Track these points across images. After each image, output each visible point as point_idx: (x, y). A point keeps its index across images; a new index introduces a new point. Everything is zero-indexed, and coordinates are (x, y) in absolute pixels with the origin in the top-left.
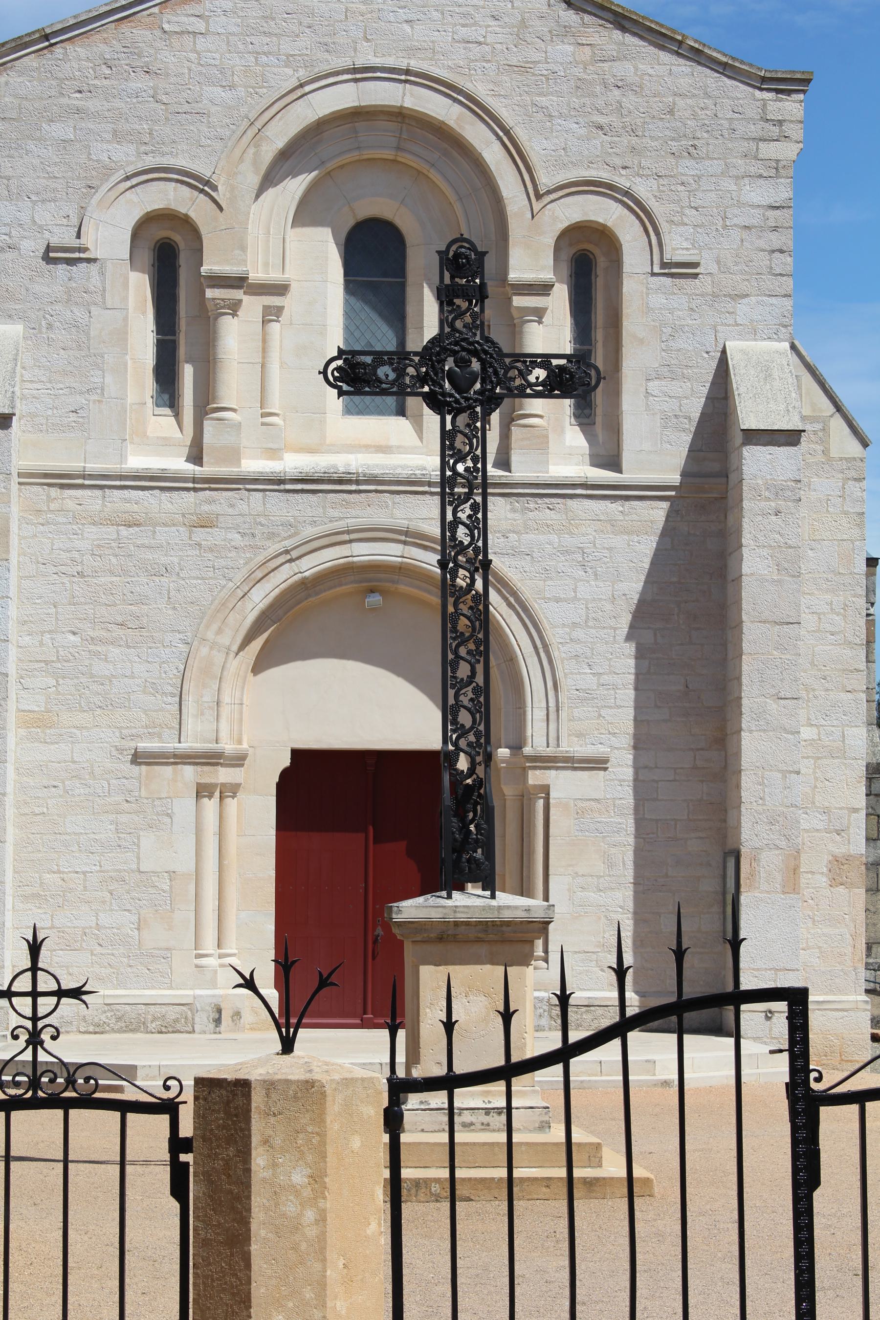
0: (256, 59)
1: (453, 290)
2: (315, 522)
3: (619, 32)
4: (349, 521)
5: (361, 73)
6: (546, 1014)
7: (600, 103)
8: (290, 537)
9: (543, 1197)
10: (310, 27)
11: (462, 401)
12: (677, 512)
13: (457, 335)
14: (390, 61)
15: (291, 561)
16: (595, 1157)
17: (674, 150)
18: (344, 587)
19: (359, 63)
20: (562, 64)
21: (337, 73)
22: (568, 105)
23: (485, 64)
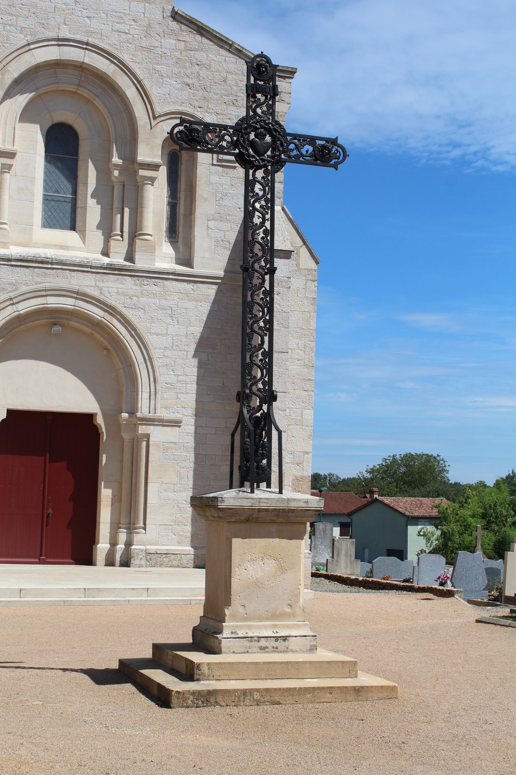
0: (4, 27)
1: (256, 88)
2: (27, 284)
3: (199, 36)
4: (46, 284)
5: (62, 42)
6: (144, 558)
7: (188, 72)
8: (13, 291)
9: (328, 701)
10: (34, 14)
11: (260, 161)
12: (221, 291)
13: (257, 117)
14: (78, 37)
15: (13, 304)
16: (353, 670)
17: (226, 101)
18: (41, 321)
19: (61, 36)
20: (169, 49)
21: (49, 40)
22: (172, 71)
23: (129, 45)
